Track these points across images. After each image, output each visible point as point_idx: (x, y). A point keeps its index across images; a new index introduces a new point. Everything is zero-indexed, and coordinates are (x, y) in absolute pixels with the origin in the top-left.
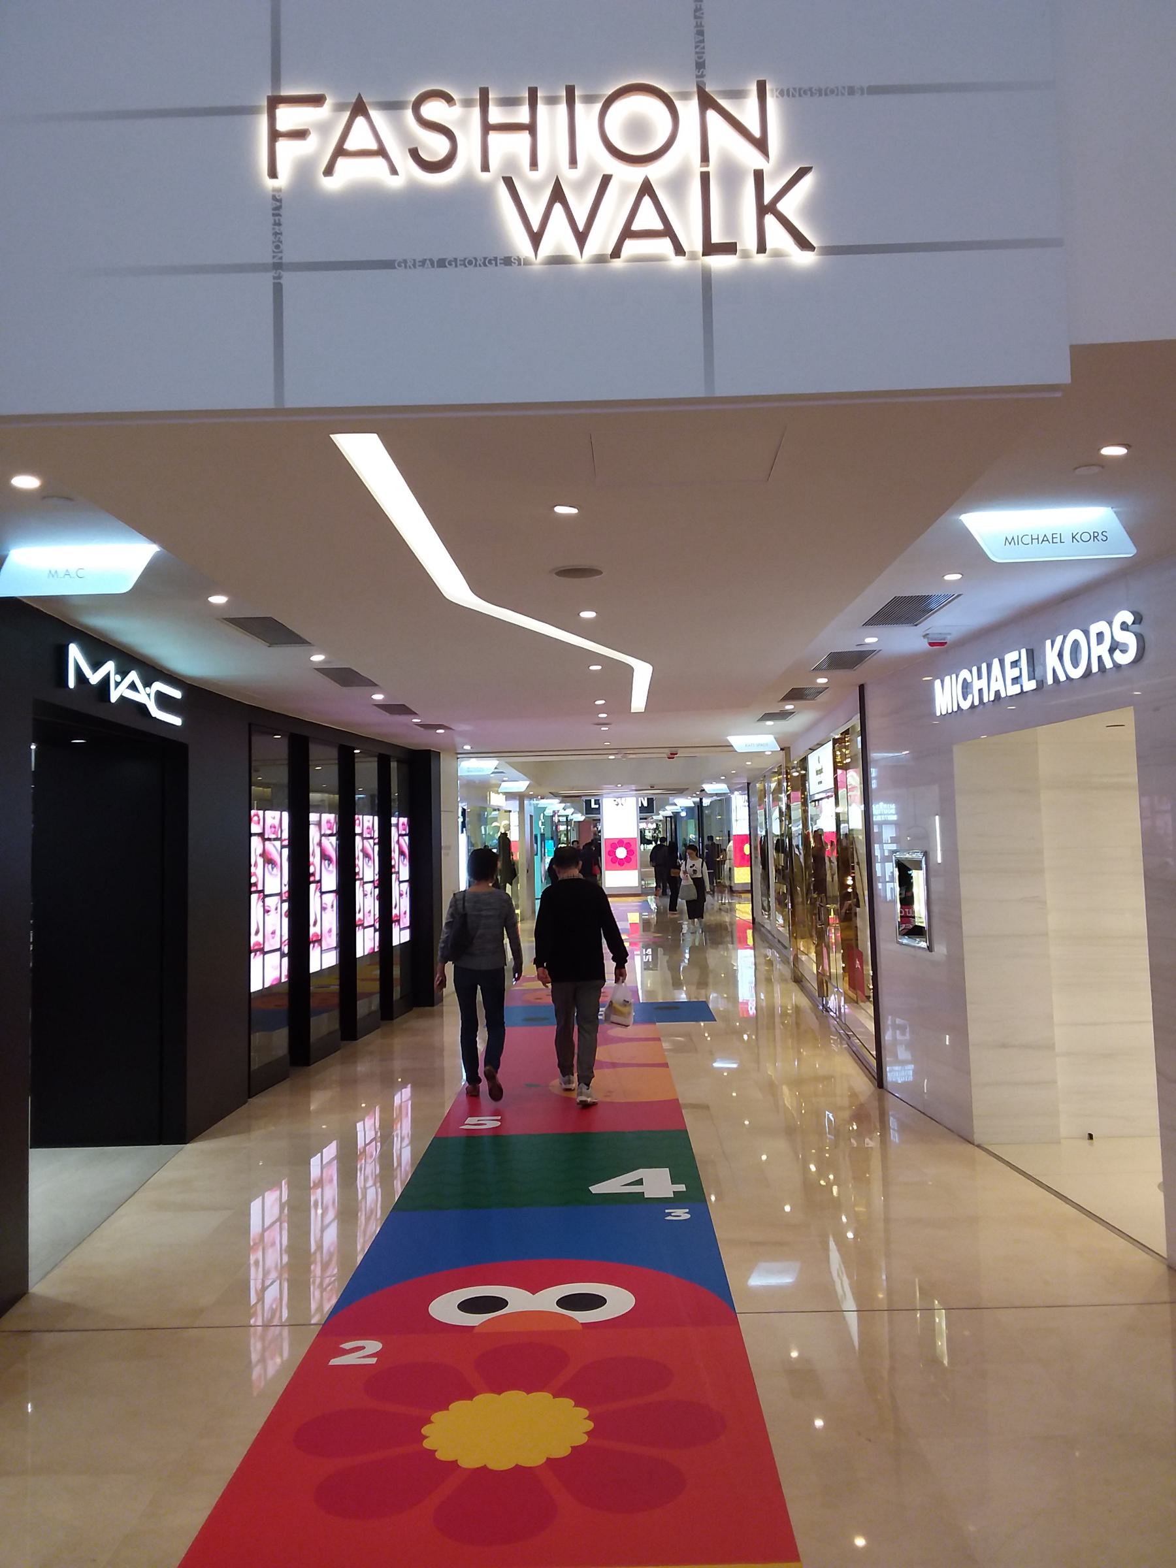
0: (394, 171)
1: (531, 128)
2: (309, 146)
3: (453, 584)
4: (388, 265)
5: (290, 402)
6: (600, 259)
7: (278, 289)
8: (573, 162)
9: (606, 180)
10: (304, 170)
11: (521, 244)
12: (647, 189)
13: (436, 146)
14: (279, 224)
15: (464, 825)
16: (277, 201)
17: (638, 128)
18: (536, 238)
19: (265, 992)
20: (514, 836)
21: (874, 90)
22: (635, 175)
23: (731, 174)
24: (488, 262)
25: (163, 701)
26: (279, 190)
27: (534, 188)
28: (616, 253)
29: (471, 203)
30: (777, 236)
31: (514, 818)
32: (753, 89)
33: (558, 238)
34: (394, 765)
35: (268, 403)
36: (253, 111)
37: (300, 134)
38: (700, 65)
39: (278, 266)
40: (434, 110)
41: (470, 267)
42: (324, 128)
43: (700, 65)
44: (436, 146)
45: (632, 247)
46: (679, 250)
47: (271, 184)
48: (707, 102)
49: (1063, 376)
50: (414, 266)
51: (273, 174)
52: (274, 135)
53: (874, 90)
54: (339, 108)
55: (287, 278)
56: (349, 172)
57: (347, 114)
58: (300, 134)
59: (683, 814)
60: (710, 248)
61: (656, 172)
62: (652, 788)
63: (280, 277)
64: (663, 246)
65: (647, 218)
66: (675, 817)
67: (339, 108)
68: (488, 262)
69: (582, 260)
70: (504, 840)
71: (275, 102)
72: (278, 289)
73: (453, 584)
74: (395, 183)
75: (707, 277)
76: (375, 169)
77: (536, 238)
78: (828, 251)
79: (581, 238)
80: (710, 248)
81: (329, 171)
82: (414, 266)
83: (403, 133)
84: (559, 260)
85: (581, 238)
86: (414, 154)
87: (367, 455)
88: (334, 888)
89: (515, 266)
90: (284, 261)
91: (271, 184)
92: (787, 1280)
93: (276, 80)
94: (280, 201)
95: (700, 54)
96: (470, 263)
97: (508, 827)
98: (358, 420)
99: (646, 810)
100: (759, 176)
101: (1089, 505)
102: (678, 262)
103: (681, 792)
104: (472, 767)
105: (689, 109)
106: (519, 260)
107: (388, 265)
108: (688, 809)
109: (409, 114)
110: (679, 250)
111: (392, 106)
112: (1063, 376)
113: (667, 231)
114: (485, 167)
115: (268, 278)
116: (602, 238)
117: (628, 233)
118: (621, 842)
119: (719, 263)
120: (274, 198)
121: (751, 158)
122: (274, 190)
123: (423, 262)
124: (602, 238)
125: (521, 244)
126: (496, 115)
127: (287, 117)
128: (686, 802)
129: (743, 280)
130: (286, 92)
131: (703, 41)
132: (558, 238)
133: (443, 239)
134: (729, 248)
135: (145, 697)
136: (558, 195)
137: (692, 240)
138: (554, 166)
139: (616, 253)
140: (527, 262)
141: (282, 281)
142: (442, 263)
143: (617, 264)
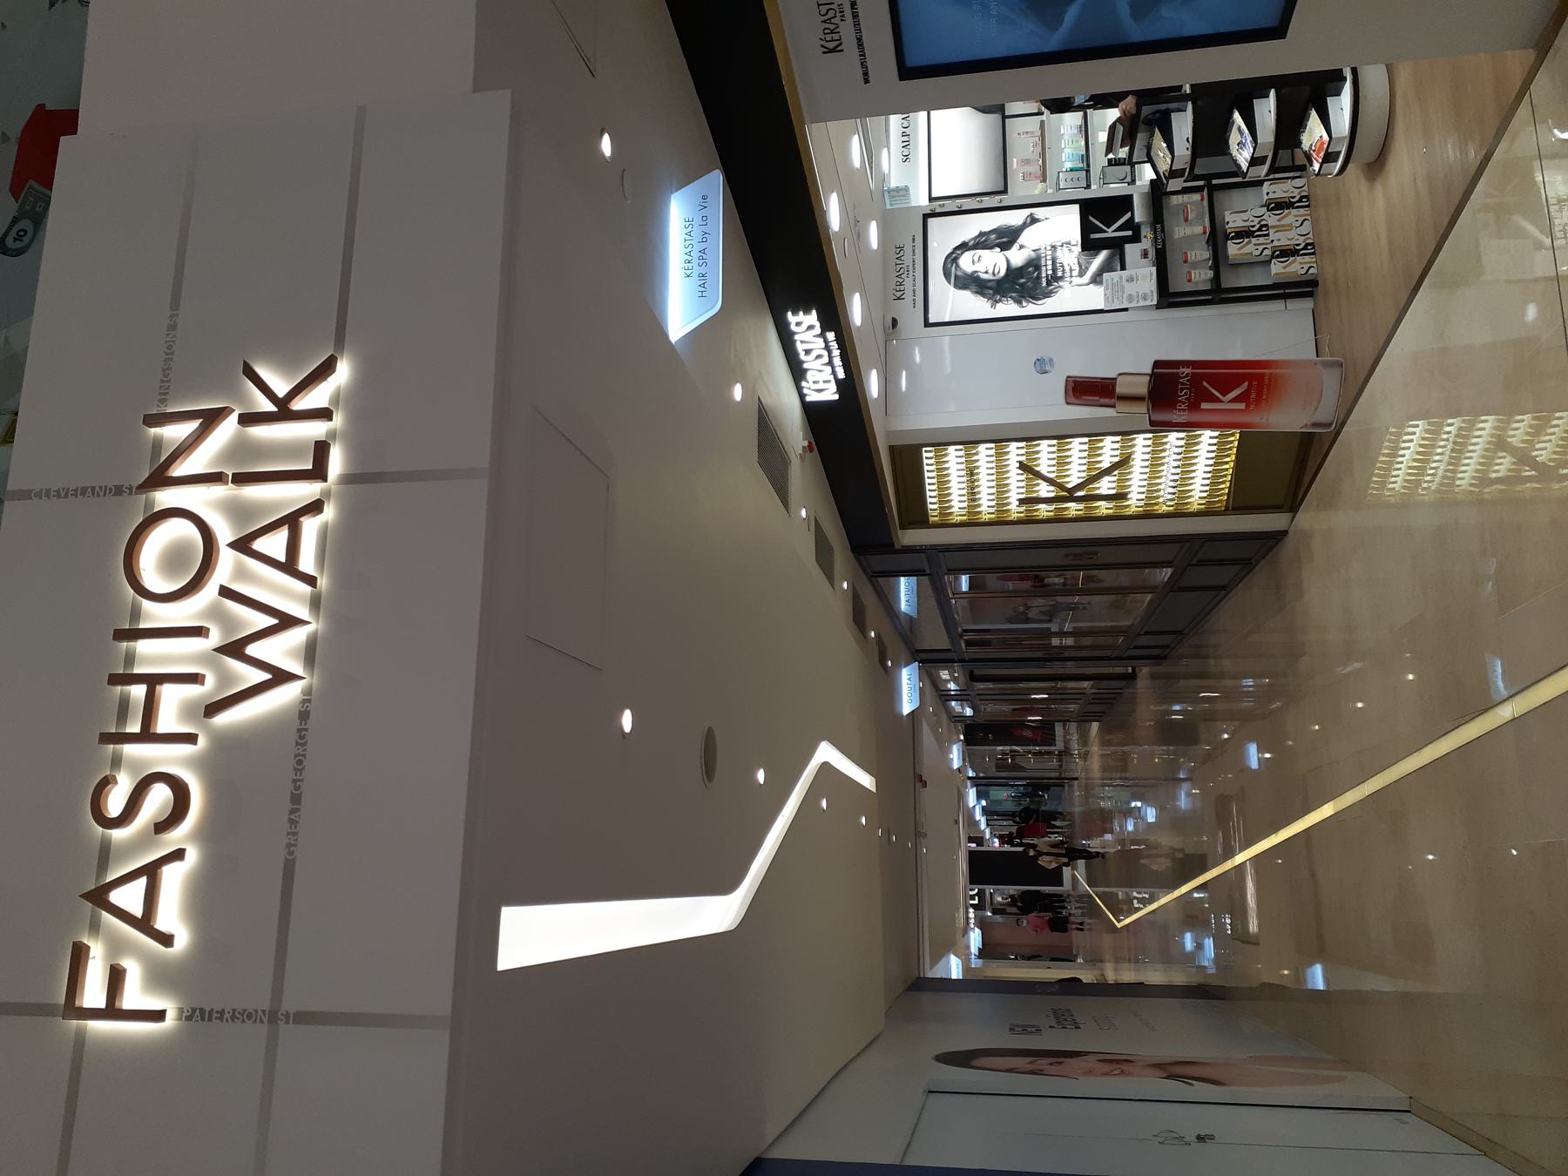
0: (178, 855)
1: (153, 681)
2: (134, 971)
3: (714, 914)
4: (289, 869)
5: (443, 1006)
6: (315, 603)
7: (303, 1018)
8: (198, 632)
9: (225, 592)
10: (159, 977)
11: (287, 695)
12: (242, 545)
13: (159, 796)
14: (222, 1013)
16: (190, 1015)
17: (173, 559)
18: (280, 677)
21: (175, 305)
22: (227, 559)
23: (240, 449)
24: (302, 740)
26: (181, 1010)
28: (310, 580)
29: (231, 761)
30: (317, 397)
32: (154, 431)
33: (280, 650)
35: (442, 1038)
36: (80, 1038)
37: (116, 978)
38: (119, 491)
39: (273, 1017)
40: (115, 804)
41: (305, 762)
42: (117, 946)
43: (119, 491)
44: (159, 796)
45: (307, 563)
46: (315, 507)
47: (171, 1015)
48: (160, 478)
49: (501, 100)
50: (295, 834)
51: (159, 1016)
52: (112, 1011)
53: (175, 305)
54: (95, 927)
55: (290, 1005)
56: (169, 917)
57: (107, 917)
58: (116, 978)
59: (984, 803)
60: (318, 472)
61: (224, 533)
62: (957, 822)
63: (287, 1015)
64: (310, 527)
65: (274, 545)
66: (985, 811)
67: (95, 927)
68: (302, 740)
71: (74, 1010)
72: (303, 1018)
73: (714, 914)
74: (192, 855)
75: (347, 479)
76: (174, 879)
77: (280, 677)
78: (340, 343)
79: (287, 622)
80: (318, 472)
81: (166, 940)
82: (295, 834)
84: (310, 653)
85: (287, 622)
86: (162, 826)
87: (534, 935)
89: (311, 707)
90: (267, 1008)
91: (171, 1015)
92: (1499, 663)
93: (44, 1010)
94: (194, 1010)
95: (106, 491)
96: (300, 762)
98: (481, 936)
100: (248, 419)
101: (667, 251)
102: (329, 513)
103: (961, 797)
105: (165, 498)
106: (304, 702)
107: (289, 869)
108: (979, 796)
109: (118, 834)
110: (315, 507)
111: (105, 854)
112: (501, 100)
113: (292, 522)
114: (190, 739)
115: (287, 1031)
116: (289, 595)
117: (289, 566)
119: (336, 463)
120: (189, 1018)
121: (228, 429)
122: (180, 1018)
123: (291, 821)
124: (289, 595)
125: (287, 695)
126: (134, 727)
127: (93, 994)
128: (971, 795)
129: (357, 442)
130: (62, 1000)
131: (93, 488)
132: (280, 650)
133: (266, 795)
134: (321, 450)
136: (235, 649)
137: (306, 491)
138: (201, 658)
139: (310, 580)
140: (308, 692)
141: (292, 1011)
142: (296, 799)
143: (323, 583)
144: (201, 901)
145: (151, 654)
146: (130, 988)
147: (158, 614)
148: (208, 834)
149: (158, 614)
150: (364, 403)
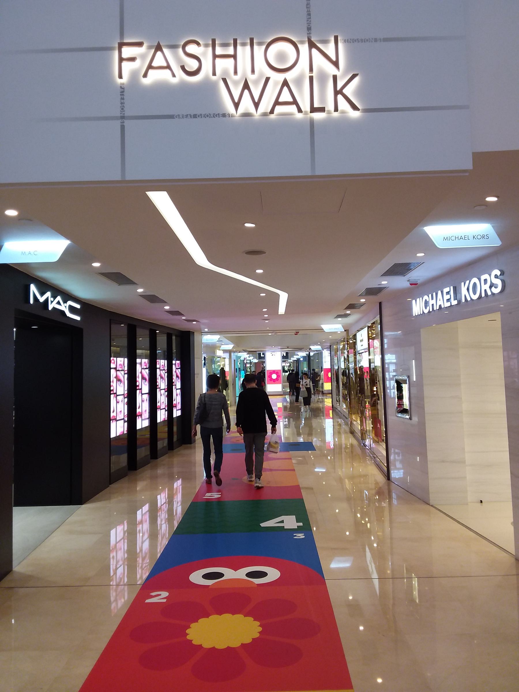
0: (174, 76)
1: (235, 56)
2: (136, 64)
4: (171, 117)
5: (128, 178)
6: (265, 114)
7: (123, 128)
8: (253, 71)
9: (268, 79)
10: (134, 75)
11: (230, 108)
12: (285, 83)
13: (193, 65)
14: (123, 99)
15: (205, 364)
16: (122, 89)
17: (281, 57)
18: (237, 105)
19: (117, 438)
20: (227, 369)
21: (386, 40)
22: (280, 77)
23: (323, 77)
24: (215, 115)
25: (72, 309)
26: (123, 84)
27: (236, 83)
28: (272, 112)
29: (208, 90)
30: (343, 104)
31: (227, 361)
32: (332, 39)
33: (246, 105)
34: (174, 338)
35: (118, 178)
36: (112, 49)
37: (133, 59)
38: (309, 29)
39: (123, 118)
40: (191, 49)
41: (208, 118)
42: (143, 57)
43: (309, 29)
44: (193, 65)
45: (279, 109)
46: (300, 110)
47: (119, 81)
48: (312, 45)
49: (469, 166)
50: (183, 117)
51: (120, 77)
52: (121, 60)
53: (386, 40)
54: (150, 47)
55: (127, 123)
56: (154, 76)
57: (153, 51)
58: (133, 59)
60: (313, 110)
61: (289, 76)
63: (123, 122)
64: (293, 109)
65: (285, 96)
67: (150, 47)
68: (215, 115)
69: (257, 115)
70: (223, 371)
71: (121, 45)
72: (123, 128)
74: (174, 81)
75: (312, 122)
76: (165, 75)
77: (237, 105)
78: (366, 111)
79: (257, 105)
80: (313, 110)
81: (145, 75)
82: (183, 117)
83: (178, 59)
84: (247, 115)
85: (257, 105)
86: (183, 68)
87: (162, 201)
88: (147, 392)
89: (227, 117)
90: (125, 115)
91: (119, 81)
93: (122, 35)
94: (124, 89)
95: (309, 24)
96: (208, 116)
97: (224, 365)
98: (158, 185)
99: (285, 358)
100: (335, 78)
102: (299, 116)
104: (208, 339)
105: (304, 48)
106: (229, 115)
107: (171, 117)
109: (180, 50)
110: (300, 110)
111: (173, 47)
112: (469, 166)
113: (295, 102)
114: (214, 74)
115: (118, 123)
116: (266, 105)
117: (277, 103)
118: (274, 372)
119: (317, 116)
120: (121, 87)
121: (331, 70)
122: (121, 84)
123: (187, 116)
124: (266, 105)
125: (230, 108)
126: (219, 51)
127: (127, 52)
129: (328, 123)
130: (126, 41)
131: (310, 18)
132: (246, 105)
133: (196, 106)
134: (322, 110)
135: (64, 307)
136: (246, 86)
137: (306, 106)
138: (244, 73)
139: (272, 112)
140: (233, 116)
141: (124, 124)
142: (195, 116)
143: (272, 116)
144: (161, 88)
145: (243, 52)
146: (138, 66)
147: (259, 51)
148: (183, 87)
149: (259, 51)
150: (342, 126)
